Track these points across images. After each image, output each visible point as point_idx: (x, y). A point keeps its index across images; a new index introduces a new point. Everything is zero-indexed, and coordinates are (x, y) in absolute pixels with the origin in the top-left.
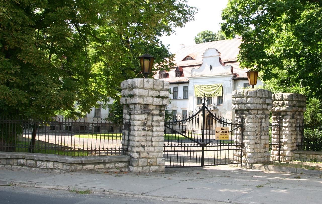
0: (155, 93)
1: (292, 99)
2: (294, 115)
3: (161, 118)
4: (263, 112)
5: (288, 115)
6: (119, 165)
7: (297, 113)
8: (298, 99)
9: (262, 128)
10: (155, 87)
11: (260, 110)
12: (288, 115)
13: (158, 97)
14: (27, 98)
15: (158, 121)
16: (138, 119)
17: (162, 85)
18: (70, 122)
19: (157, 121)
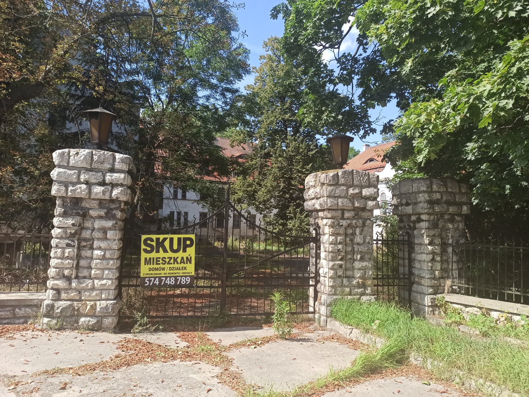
0: (94, 177)
1: (432, 189)
2: (438, 220)
3: (109, 224)
4: (356, 215)
5: (423, 221)
6: (21, 312)
7: (446, 217)
8: (447, 189)
9: (355, 246)
10: (94, 166)
11: (349, 210)
12: (423, 221)
13: (103, 183)
14: (294, 226)
15: (104, 231)
16: (234, 232)
17: (111, 161)
18: (380, 240)
19: (99, 229)
